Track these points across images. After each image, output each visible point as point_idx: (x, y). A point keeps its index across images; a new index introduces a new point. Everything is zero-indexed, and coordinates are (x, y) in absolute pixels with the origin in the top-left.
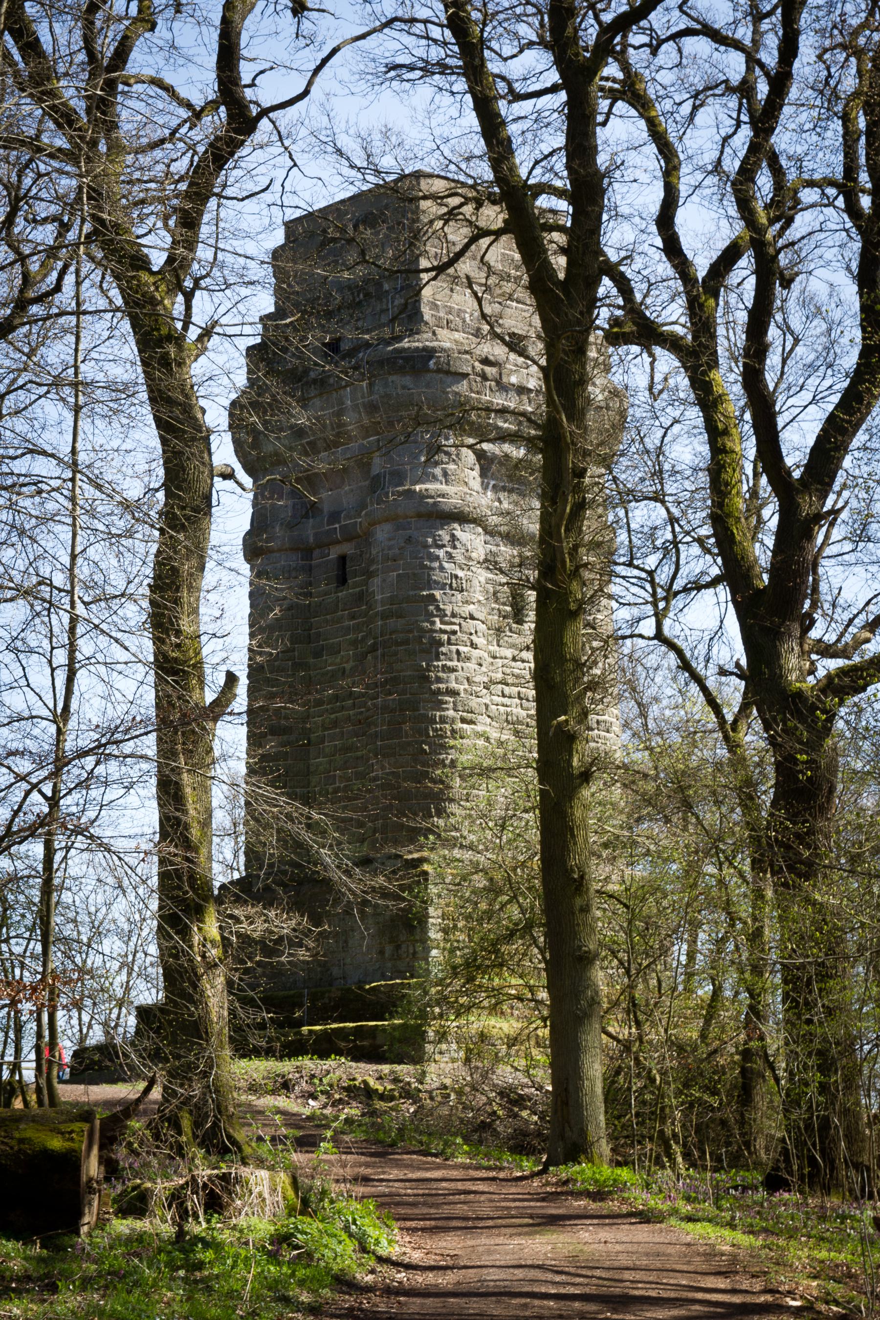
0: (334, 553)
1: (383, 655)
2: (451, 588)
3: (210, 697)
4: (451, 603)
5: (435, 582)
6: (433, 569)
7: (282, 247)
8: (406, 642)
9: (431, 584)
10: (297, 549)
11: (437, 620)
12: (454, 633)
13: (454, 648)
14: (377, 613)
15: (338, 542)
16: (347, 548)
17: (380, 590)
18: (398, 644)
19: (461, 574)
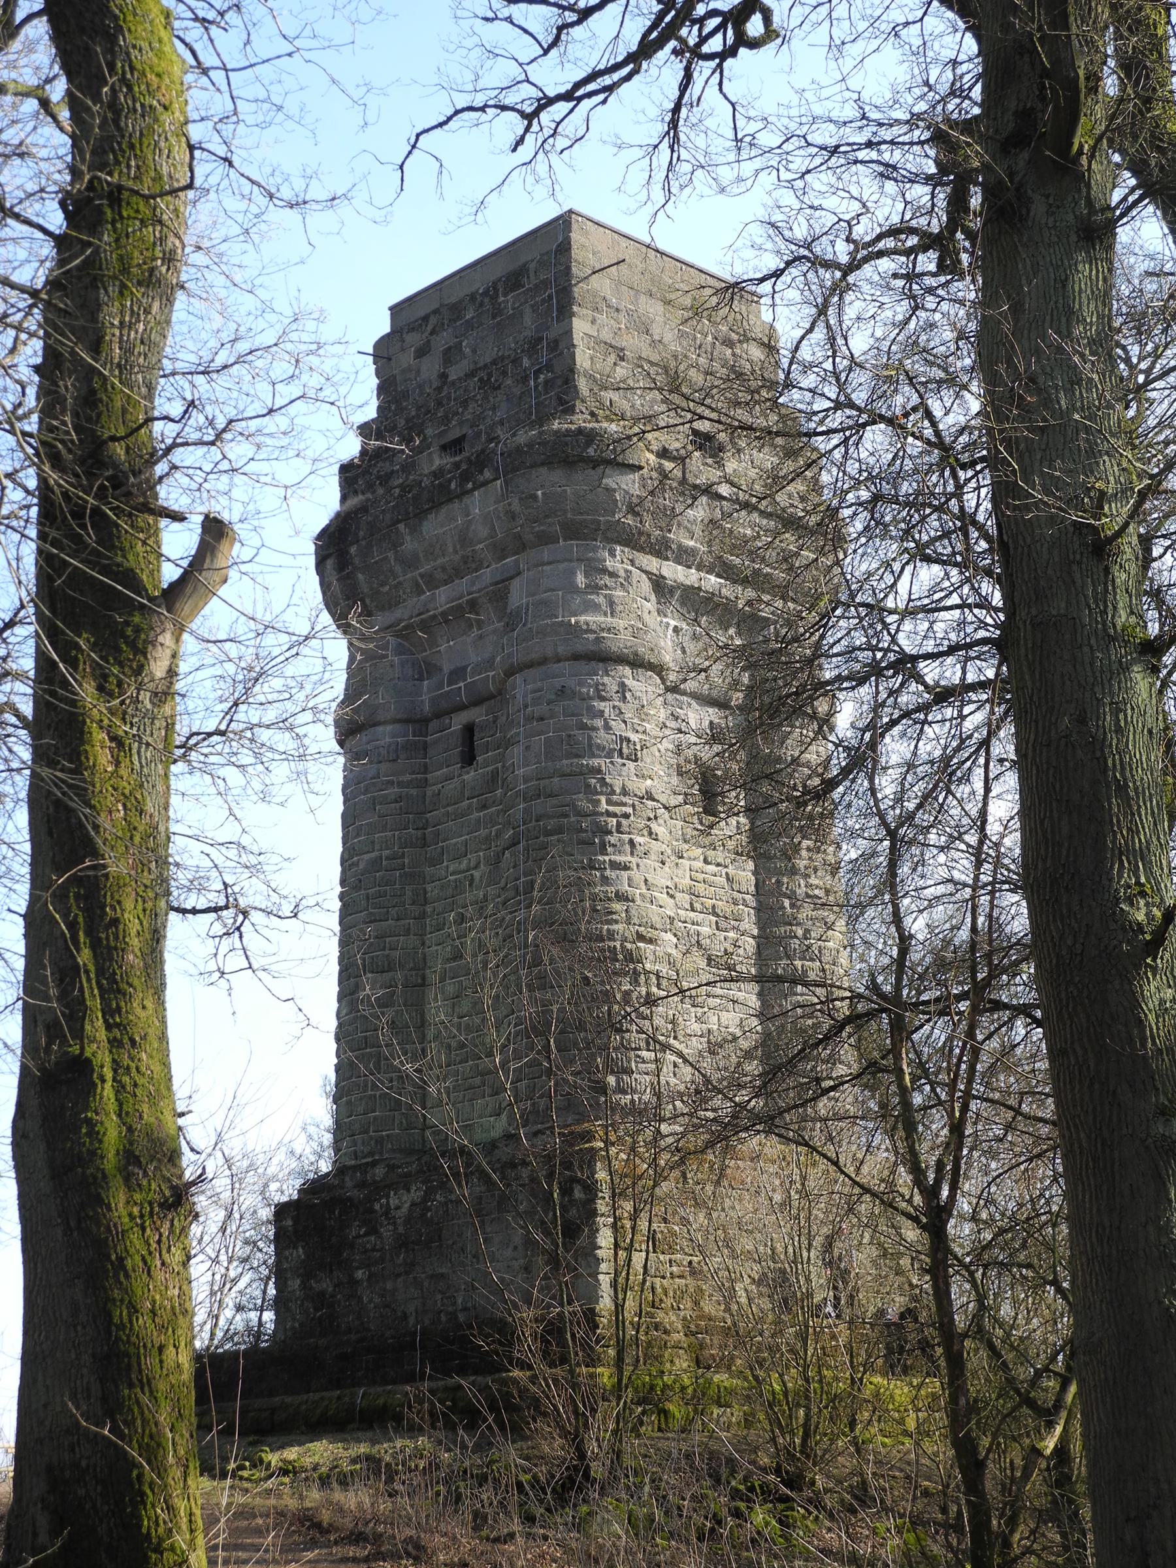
0: (458, 722)
1: (527, 849)
2: (621, 755)
3: (170, 573)
4: (623, 775)
5: (599, 747)
6: (595, 729)
7: (388, 335)
8: (559, 830)
9: (592, 749)
10: (407, 721)
11: (603, 799)
12: (626, 816)
13: (626, 837)
14: (518, 794)
15: (462, 707)
16: (477, 715)
17: (522, 766)
18: (548, 834)
19: (634, 737)
